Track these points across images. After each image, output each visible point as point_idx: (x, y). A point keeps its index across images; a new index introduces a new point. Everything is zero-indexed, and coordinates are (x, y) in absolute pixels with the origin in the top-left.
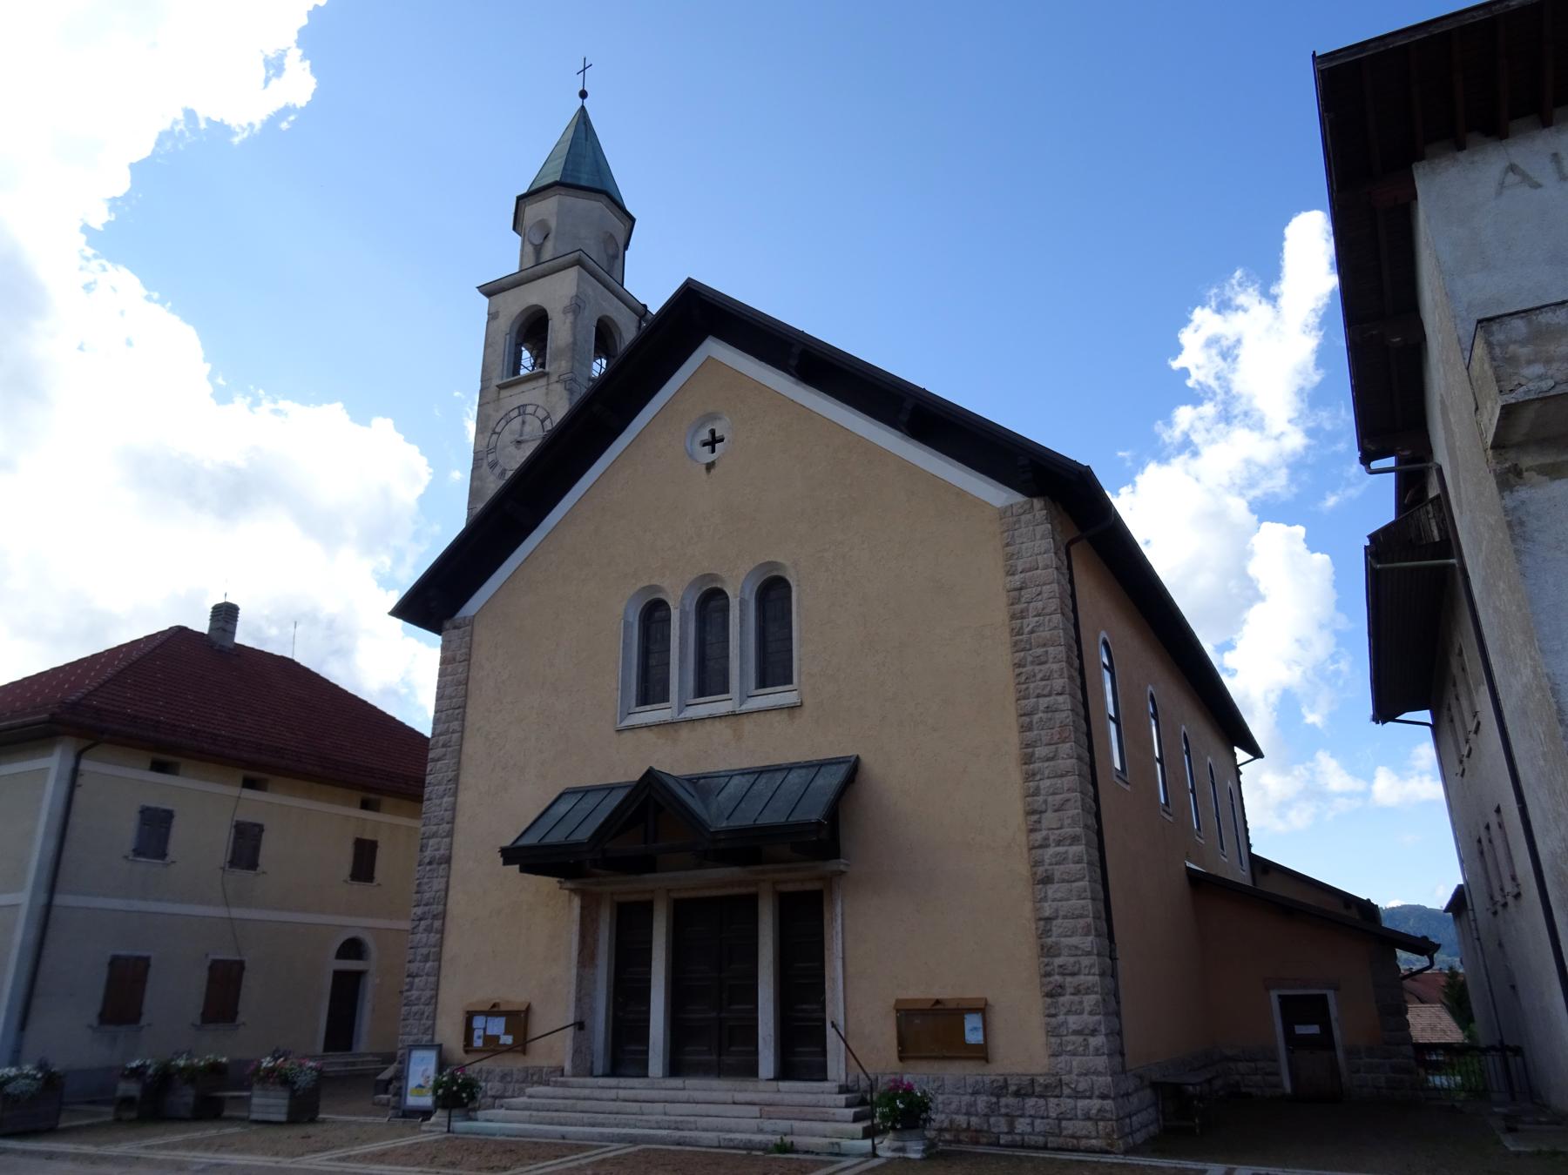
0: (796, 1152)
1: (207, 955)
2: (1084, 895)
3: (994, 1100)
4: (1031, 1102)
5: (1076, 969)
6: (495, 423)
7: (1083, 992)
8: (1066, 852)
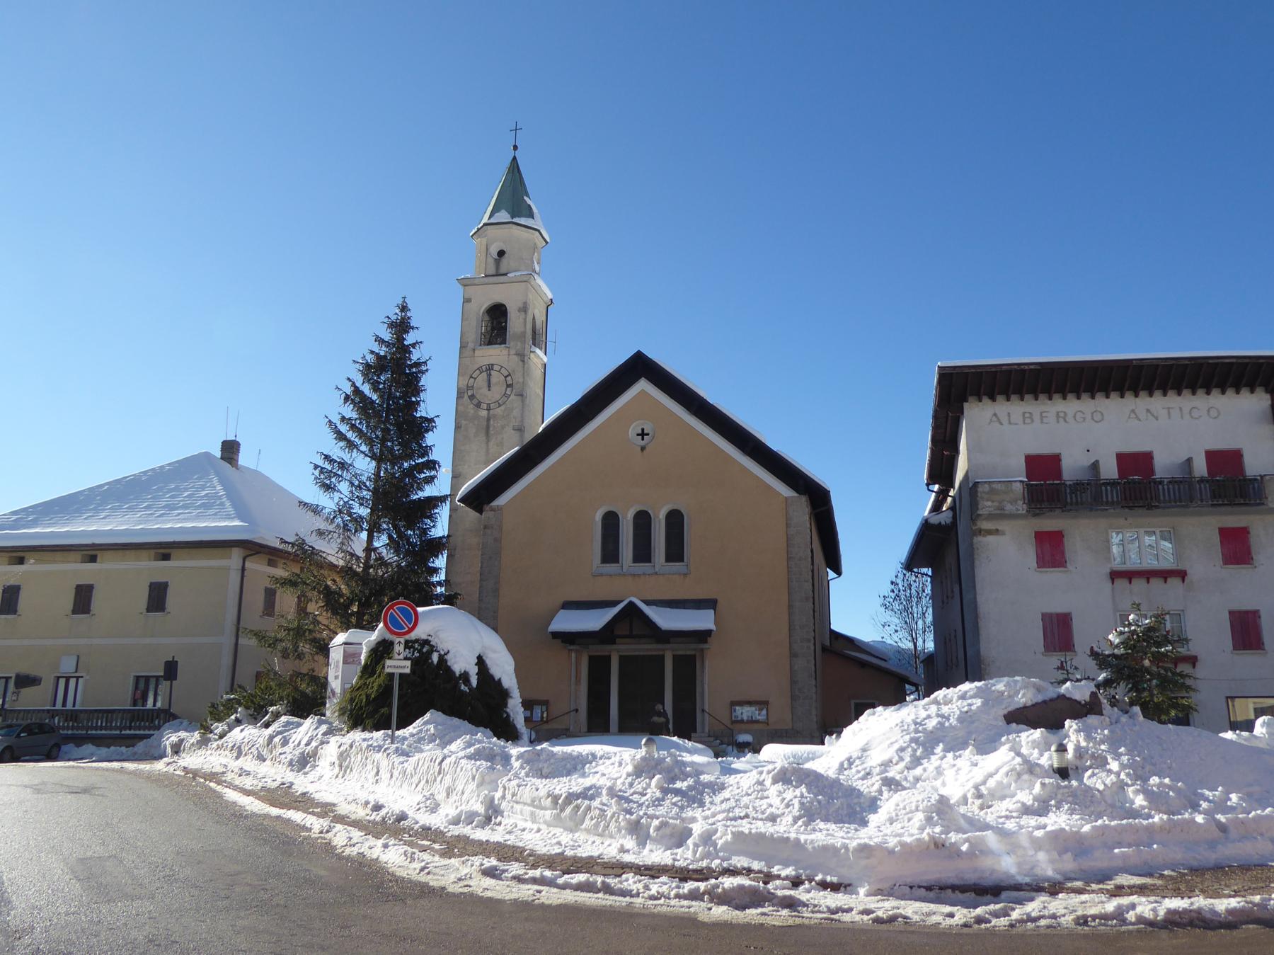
6: (811, 593)
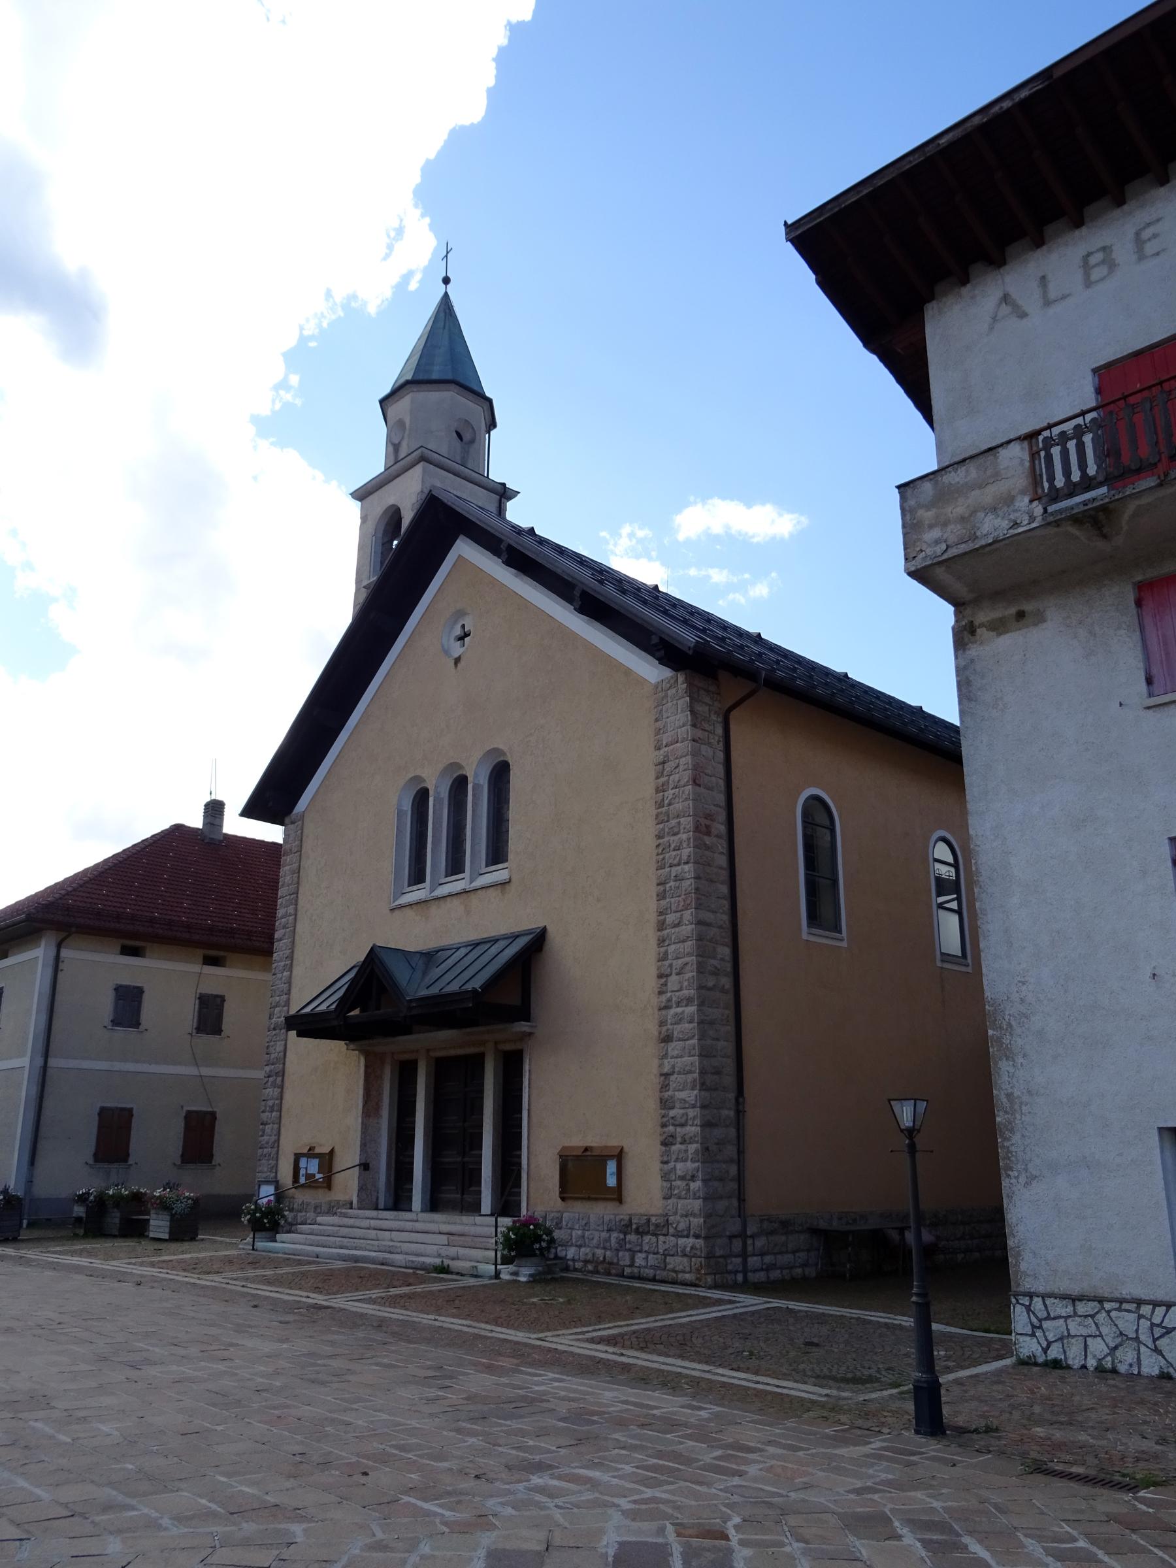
0: (452, 1273)
1: (182, 1107)
2: (693, 1052)
3: (622, 1236)
4: (647, 1238)
5: (683, 1121)
7: (688, 1141)
8: (683, 1012)
